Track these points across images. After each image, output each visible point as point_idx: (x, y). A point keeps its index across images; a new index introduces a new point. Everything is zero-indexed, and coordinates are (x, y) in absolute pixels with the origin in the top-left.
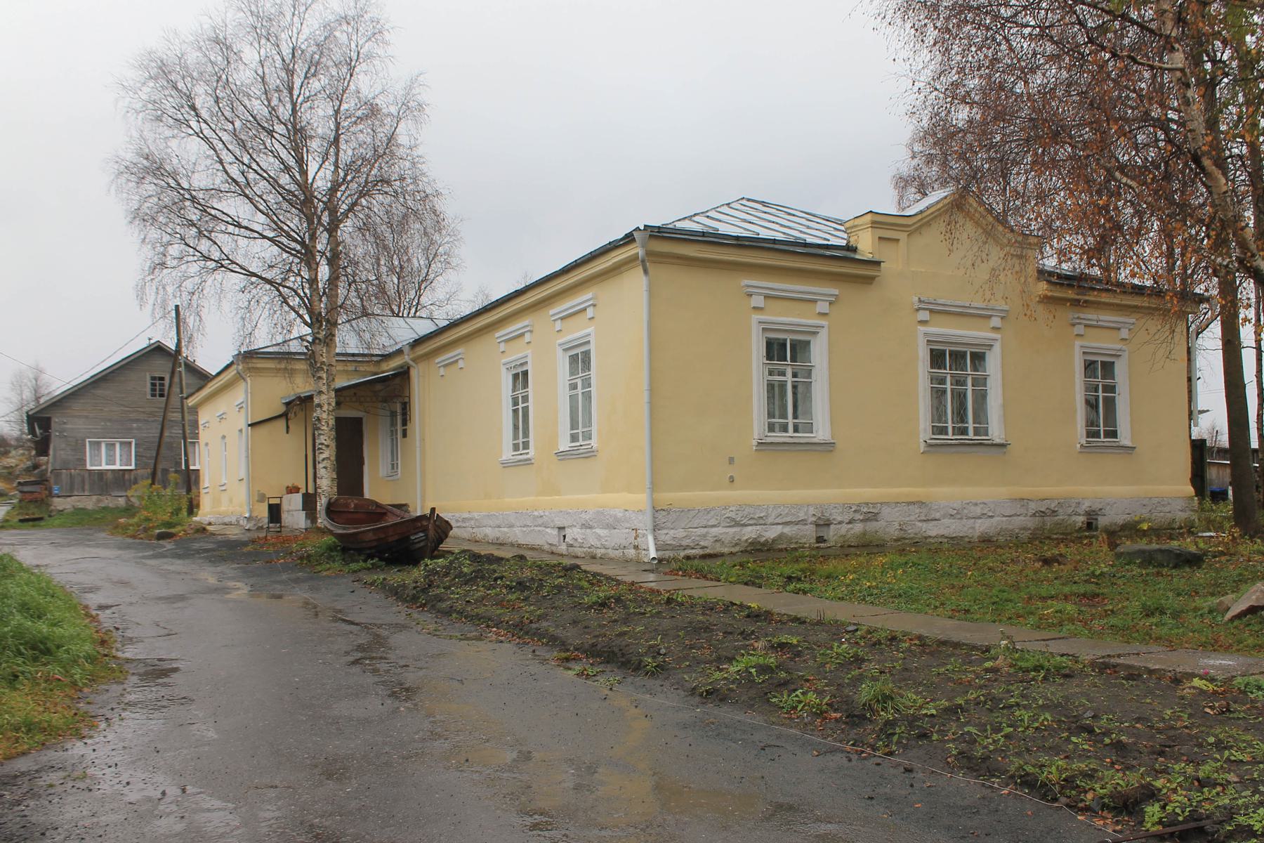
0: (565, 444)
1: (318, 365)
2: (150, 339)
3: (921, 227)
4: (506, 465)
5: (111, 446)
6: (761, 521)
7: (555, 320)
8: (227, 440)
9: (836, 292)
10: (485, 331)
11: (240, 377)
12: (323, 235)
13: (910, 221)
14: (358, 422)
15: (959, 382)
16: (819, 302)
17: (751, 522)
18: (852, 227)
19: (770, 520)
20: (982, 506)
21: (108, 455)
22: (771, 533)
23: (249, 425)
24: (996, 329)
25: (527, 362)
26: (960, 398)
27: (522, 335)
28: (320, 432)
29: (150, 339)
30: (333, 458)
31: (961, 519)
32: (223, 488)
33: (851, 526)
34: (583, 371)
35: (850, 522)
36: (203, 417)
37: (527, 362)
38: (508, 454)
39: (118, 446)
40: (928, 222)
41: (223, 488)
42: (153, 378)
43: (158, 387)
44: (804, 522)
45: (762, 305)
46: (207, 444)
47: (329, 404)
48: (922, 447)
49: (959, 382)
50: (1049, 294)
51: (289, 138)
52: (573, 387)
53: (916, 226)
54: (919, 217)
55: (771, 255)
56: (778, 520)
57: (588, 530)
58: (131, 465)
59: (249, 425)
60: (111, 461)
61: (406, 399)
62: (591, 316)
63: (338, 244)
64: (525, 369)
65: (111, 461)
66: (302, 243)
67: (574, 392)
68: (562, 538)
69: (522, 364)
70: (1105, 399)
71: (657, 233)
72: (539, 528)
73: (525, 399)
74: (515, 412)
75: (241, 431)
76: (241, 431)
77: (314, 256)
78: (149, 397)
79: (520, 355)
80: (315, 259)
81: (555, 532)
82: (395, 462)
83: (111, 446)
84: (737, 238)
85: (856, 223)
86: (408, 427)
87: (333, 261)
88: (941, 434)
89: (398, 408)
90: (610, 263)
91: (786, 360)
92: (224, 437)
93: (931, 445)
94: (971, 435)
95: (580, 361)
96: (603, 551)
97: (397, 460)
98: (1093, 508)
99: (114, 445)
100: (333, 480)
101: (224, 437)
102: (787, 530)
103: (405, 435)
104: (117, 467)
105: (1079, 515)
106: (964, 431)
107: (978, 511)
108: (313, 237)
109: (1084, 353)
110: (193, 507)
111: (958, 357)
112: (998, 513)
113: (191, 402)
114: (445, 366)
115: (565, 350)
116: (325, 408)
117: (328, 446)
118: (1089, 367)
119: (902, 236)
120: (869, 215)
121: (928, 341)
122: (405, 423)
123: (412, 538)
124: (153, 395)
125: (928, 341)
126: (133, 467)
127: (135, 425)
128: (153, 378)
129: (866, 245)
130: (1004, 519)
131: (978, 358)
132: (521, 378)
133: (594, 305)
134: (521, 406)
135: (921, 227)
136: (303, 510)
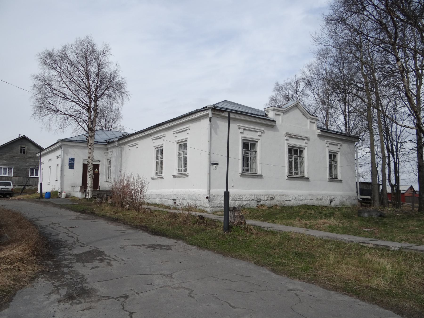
0: (176, 173)
1: (90, 144)
2: (20, 135)
3: (286, 111)
4: (153, 179)
5: (5, 169)
6: (241, 199)
8: (51, 168)
9: (264, 129)
11: (60, 147)
12: (93, 103)
13: (283, 110)
15: (296, 159)
16: (259, 132)
17: (238, 199)
18: (267, 110)
19: (244, 199)
20: (302, 196)
21: (4, 172)
22: (245, 203)
24: (306, 143)
25: (163, 146)
26: (296, 163)
28: (89, 166)
29: (20, 135)
31: (297, 200)
32: (49, 184)
33: (266, 202)
35: (266, 201)
37: (163, 146)
38: (154, 175)
39: (7, 169)
40: (288, 110)
43: (23, 151)
44: (253, 200)
45: (242, 132)
48: (286, 178)
49: (296, 159)
50: (321, 134)
51: (85, 72)
52: (179, 155)
53: (285, 111)
54: (286, 109)
55: (244, 116)
56: (246, 199)
57: (184, 201)
58: (11, 175)
60: (5, 173)
63: (97, 106)
64: (162, 148)
65: (5, 173)
66: (87, 105)
67: (180, 156)
68: (174, 203)
69: (160, 147)
71: (63, 140)
72: (165, 200)
73: (111, 167)
74: (157, 163)
76: (58, 165)
77: (90, 109)
78: (19, 153)
79: (161, 144)
80: (90, 110)
81: (172, 201)
83: (5, 169)
84: (236, 111)
85: (268, 109)
87: (95, 111)
88: (291, 174)
90: (197, 116)
91: (248, 149)
93: (288, 177)
94: (299, 175)
95: (183, 146)
98: (332, 198)
99: (6, 168)
101: (50, 167)
102: (248, 202)
104: (7, 176)
105: (328, 200)
106: (297, 174)
107: (301, 198)
108: (91, 103)
109: (329, 152)
111: (296, 152)
112: (306, 199)
117: (91, 171)
118: (330, 156)
119: (281, 114)
120: (273, 107)
121: (288, 146)
124: (21, 153)
125: (288, 146)
126: (12, 176)
127: (14, 162)
128: (21, 147)
129: (271, 115)
130: (308, 201)
131: (301, 151)
133: (189, 129)
134: (159, 160)
135: (286, 111)
136: (80, 192)
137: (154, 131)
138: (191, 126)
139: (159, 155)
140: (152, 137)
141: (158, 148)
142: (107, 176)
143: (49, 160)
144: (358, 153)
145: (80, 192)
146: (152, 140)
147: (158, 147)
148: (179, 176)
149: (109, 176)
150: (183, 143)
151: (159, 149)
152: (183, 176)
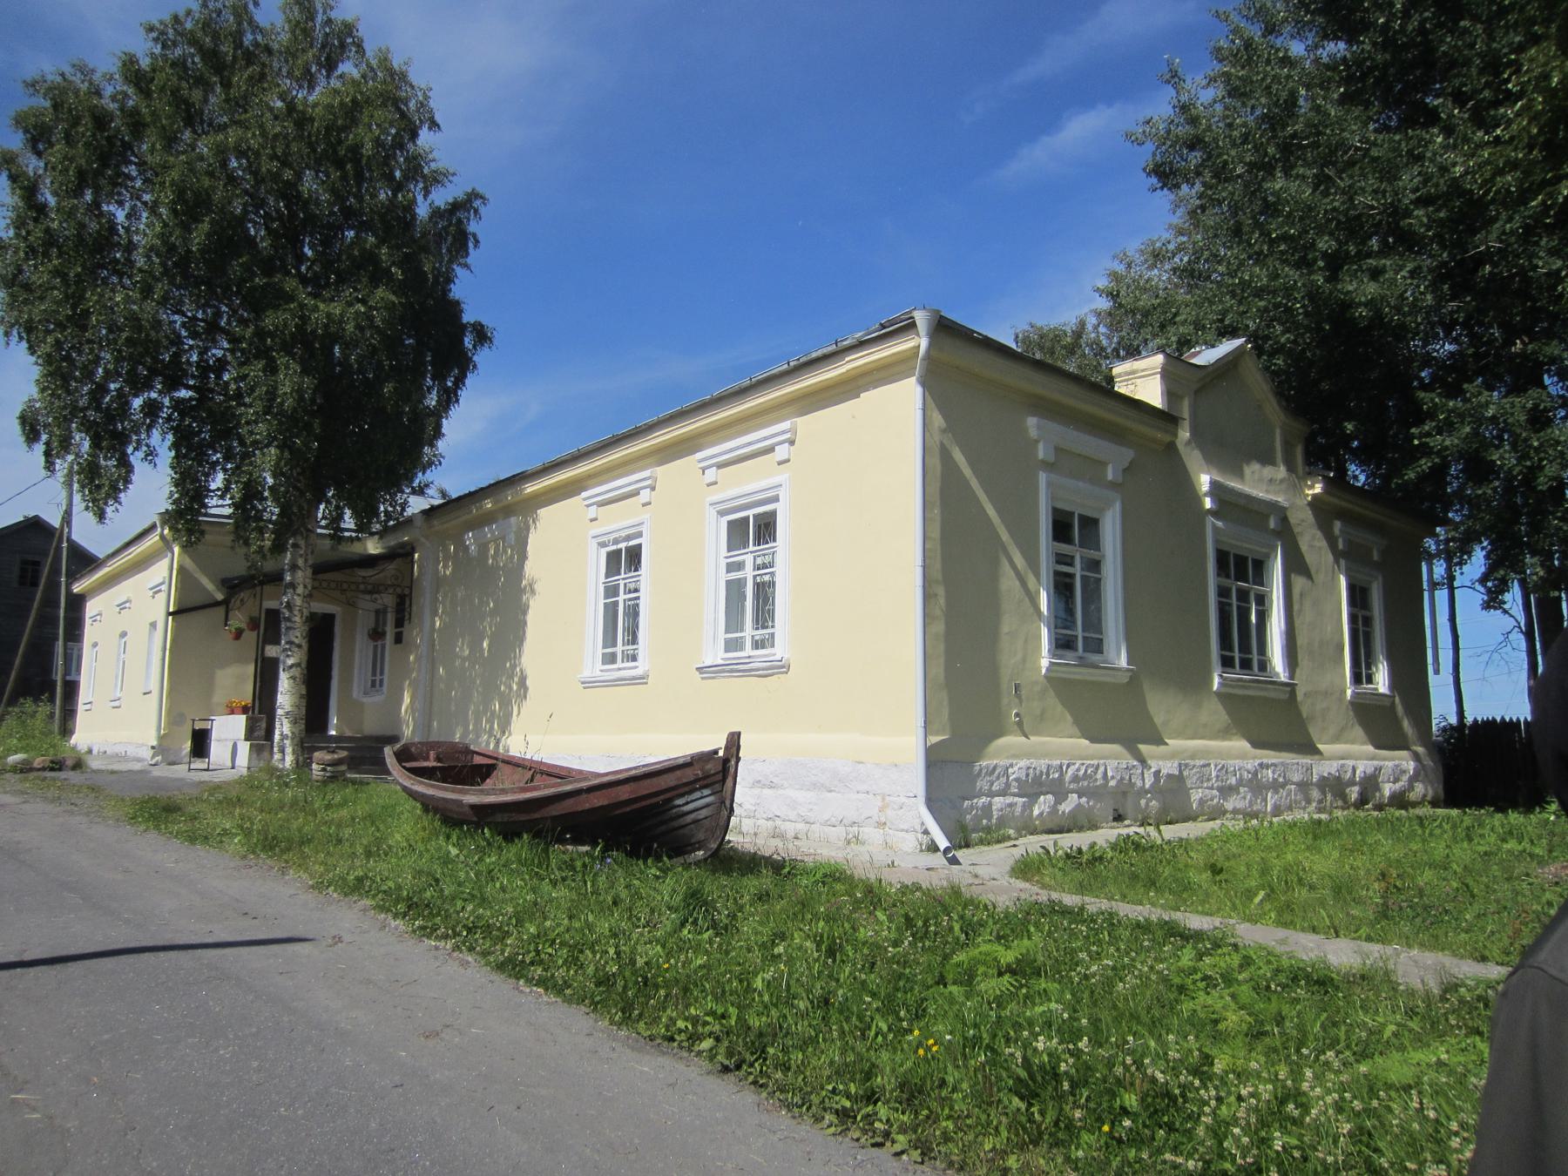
0: (715, 655)
4: (588, 684)
7: (588, 506)
10: (620, 471)
14: (328, 620)
23: (170, 614)
27: (636, 493)
30: (304, 665)
32: (116, 704)
34: (758, 542)
36: (91, 608)
41: (116, 704)
42: (24, 562)
46: (95, 645)
47: (305, 587)
57: (767, 791)
59: (170, 614)
61: (407, 591)
62: (594, 516)
69: (628, 538)
70: (1231, 649)
75: (153, 625)
79: (764, 484)
82: (378, 678)
86: (406, 630)
89: (388, 600)
92: (124, 634)
96: (801, 826)
97: (382, 673)
100: (302, 696)
101: (124, 634)
103: (398, 639)
110: (67, 730)
113: (77, 588)
114: (720, 466)
115: (722, 513)
116: (300, 590)
122: (399, 623)
123: (679, 802)
132: (625, 559)
136: (246, 740)
137: (778, 394)
138: (809, 425)
139: (622, 579)
140: (700, 455)
141: (616, 541)
142: (370, 673)
143: (122, 606)
144: (247, 698)
145: (246, 740)
146: (588, 506)
147: (612, 537)
148: (724, 671)
149: (374, 674)
150: (750, 513)
151: (622, 546)
152: (758, 670)
